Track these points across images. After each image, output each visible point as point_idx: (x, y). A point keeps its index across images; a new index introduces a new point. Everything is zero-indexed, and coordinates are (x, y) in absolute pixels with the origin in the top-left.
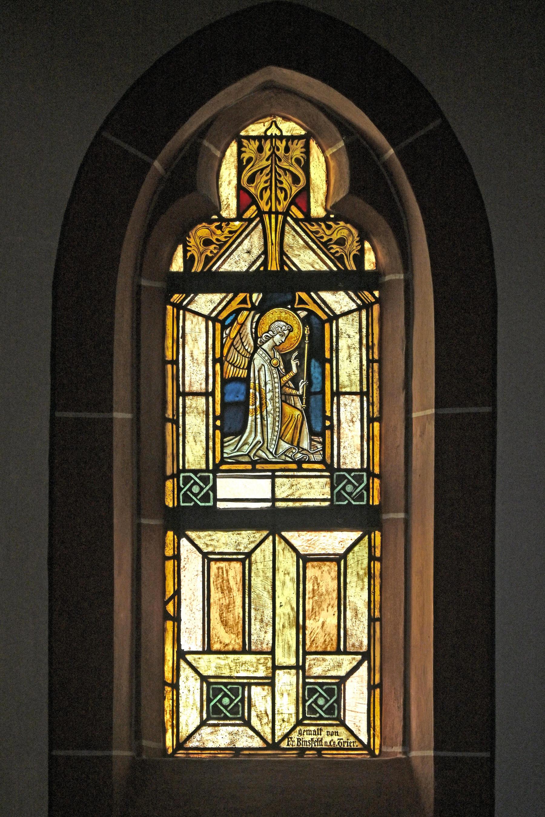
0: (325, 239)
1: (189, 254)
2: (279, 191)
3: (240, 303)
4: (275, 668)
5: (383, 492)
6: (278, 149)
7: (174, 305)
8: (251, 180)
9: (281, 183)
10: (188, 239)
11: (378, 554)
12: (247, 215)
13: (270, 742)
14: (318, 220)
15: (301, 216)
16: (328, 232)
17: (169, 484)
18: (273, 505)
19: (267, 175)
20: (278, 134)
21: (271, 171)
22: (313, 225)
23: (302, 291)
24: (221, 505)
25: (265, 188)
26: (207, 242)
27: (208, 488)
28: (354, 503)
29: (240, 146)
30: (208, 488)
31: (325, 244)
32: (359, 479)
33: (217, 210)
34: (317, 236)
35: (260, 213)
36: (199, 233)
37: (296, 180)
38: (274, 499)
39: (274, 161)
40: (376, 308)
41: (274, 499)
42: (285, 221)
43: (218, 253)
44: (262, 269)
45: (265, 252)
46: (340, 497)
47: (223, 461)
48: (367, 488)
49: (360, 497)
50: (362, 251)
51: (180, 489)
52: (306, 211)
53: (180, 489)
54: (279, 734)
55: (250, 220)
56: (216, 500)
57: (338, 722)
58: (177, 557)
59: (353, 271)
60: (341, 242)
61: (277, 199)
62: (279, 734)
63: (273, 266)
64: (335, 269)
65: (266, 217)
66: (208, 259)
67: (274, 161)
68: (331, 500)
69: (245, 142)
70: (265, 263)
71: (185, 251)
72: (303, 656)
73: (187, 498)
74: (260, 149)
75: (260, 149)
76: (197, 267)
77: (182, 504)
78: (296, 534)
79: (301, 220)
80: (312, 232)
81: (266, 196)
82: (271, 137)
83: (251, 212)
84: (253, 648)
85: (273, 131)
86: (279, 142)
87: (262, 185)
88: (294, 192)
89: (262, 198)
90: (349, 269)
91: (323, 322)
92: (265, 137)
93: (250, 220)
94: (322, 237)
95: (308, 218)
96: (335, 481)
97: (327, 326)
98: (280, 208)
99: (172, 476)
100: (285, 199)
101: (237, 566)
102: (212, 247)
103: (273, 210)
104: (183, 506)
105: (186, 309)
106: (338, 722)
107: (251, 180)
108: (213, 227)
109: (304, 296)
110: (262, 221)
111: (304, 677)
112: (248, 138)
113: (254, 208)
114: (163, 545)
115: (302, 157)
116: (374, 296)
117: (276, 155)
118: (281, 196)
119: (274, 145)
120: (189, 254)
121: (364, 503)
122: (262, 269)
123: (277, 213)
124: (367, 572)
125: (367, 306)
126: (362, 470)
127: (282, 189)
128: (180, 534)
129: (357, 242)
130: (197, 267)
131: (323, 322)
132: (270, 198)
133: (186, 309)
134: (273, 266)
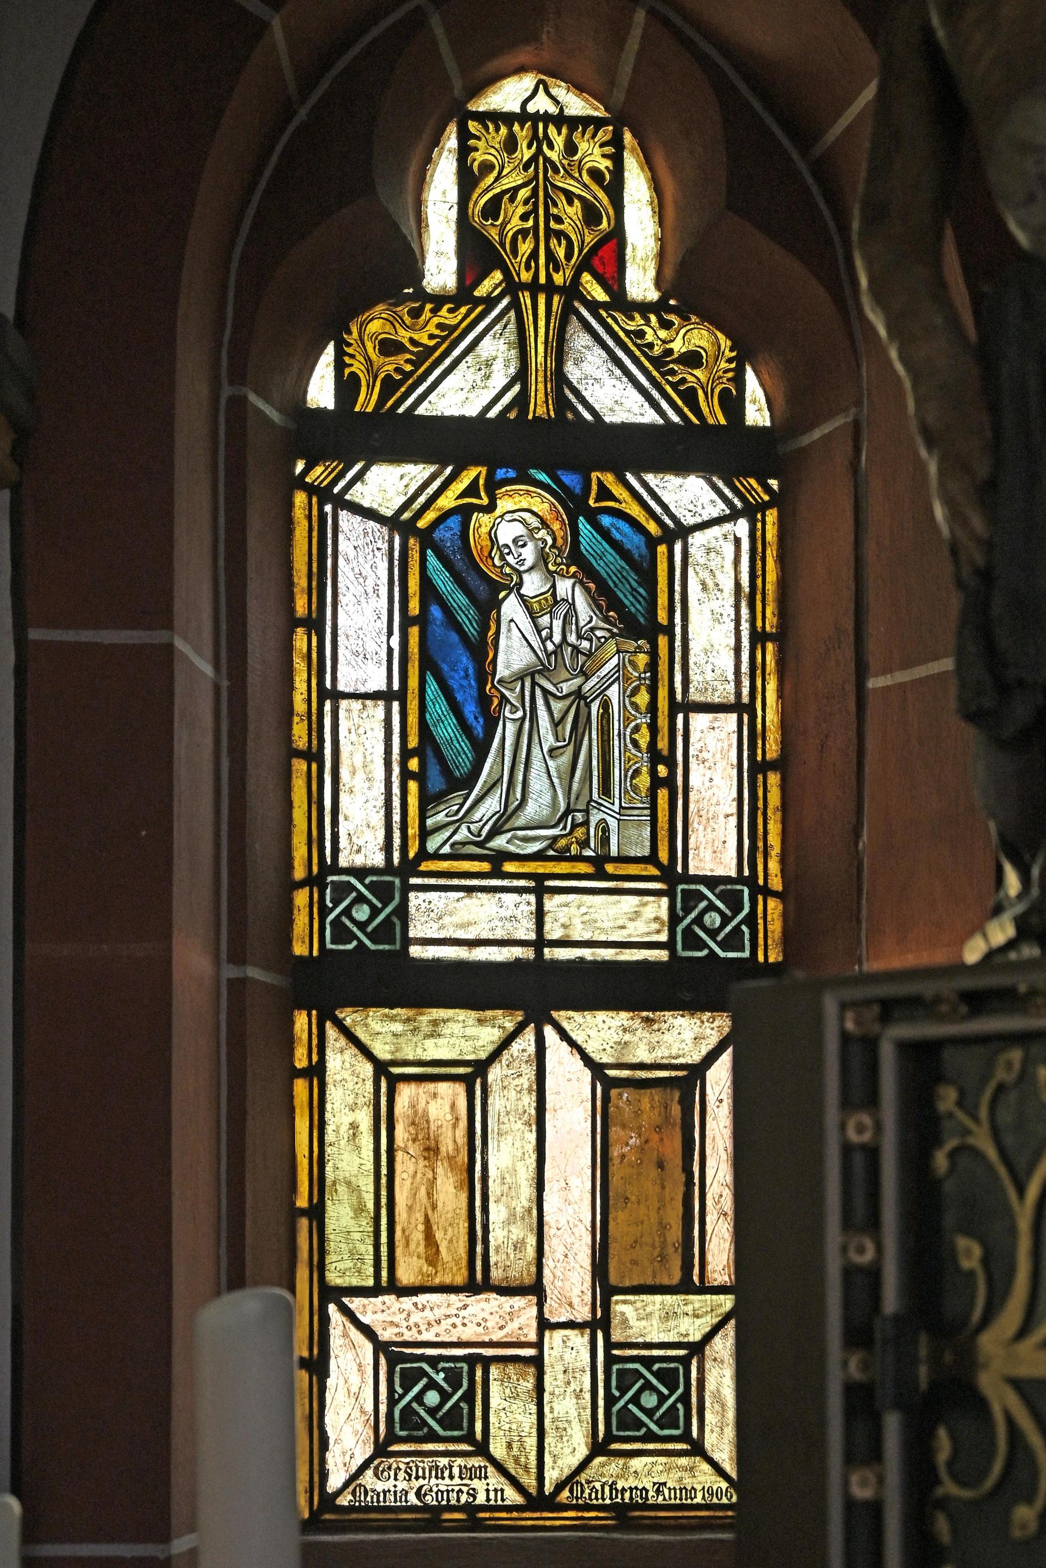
0: (657, 351)
1: (347, 371)
2: (554, 242)
3: (461, 496)
4: (544, 1325)
5: (791, 858)
6: (551, 147)
7: (311, 490)
8: (492, 209)
9: (559, 220)
10: (345, 336)
11: (304, 1223)
12: (481, 291)
13: (533, 1491)
14: (644, 308)
15: (600, 295)
16: (663, 334)
17: (301, 898)
18: (539, 953)
19: (526, 202)
20: (553, 110)
21: (535, 192)
22: (632, 319)
23: (602, 469)
24: (415, 951)
25: (524, 233)
26: (389, 347)
27: (389, 910)
28: (722, 954)
29: (464, 136)
30: (389, 910)
31: (658, 362)
32: (734, 902)
33: (416, 275)
34: (639, 341)
35: (512, 287)
36: (374, 327)
37: (591, 215)
38: (540, 943)
39: (541, 171)
40: (772, 516)
41: (540, 943)
42: (568, 311)
43: (412, 373)
44: (512, 415)
45: (522, 376)
46: (692, 941)
47: (423, 855)
48: (751, 920)
49: (733, 941)
50: (739, 381)
51: (324, 911)
52: (615, 283)
53: (324, 911)
54: (552, 1476)
55: (490, 302)
56: (407, 942)
57: (685, 1446)
58: (317, 1071)
59: (720, 426)
60: (692, 359)
61: (550, 256)
62: (552, 1476)
63: (540, 406)
64: (675, 419)
65: (525, 298)
66: (389, 386)
67: (541, 171)
68: (669, 945)
69: (473, 126)
70: (522, 400)
71: (340, 365)
72: (442, 1532)
73: (341, 933)
74: (511, 145)
75: (511, 145)
76: (366, 401)
77: (329, 946)
78: (576, 1015)
79: (604, 305)
80: (627, 333)
81: (525, 248)
82: (536, 117)
83: (490, 284)
84: (496, 1274)
85: (541, 104)
86: (555, 131)
87: (515, 224)
88: (590, 239)
89: (515, 251)
90: (711, 421)
91: (652, 543)
92: (523, 117)
93: (490, 302)
94: (651, 346)
95: (620, 302)
96: (679, 905)
97: (662, 549)
98: (558, 279)
99: (309, 881)
100: (569, 256)
101: (406, 1093)
102: (401, 359)
103: (542, 280)
104: (332, 950)
105: (341, 503)
106: (685, 1446)
107: (492, 209)
108: (403, 310)
109: (609, 479)
110: (515, 305)
111: (609, 1345)
112: (483, 117)
113: (497, 276)
114: (289, 1042)
115: (607, 168)
116: (768, 489)
117: (547, 160)
118: (561, 252)
119: (541, 135)
120: (347, 371)
121: (746, 954)
122: (512, 415)
123: (550, 288)
124: (683, 1297)
125: (751, 511)
126: (740, 879)
127: (560, 234)
128: (327, 1015)
129: (730, 361)
130: (366, 401)
131: (652, 543)
132: (534, 255)
133: (341, 503)
134: (540, 406)
